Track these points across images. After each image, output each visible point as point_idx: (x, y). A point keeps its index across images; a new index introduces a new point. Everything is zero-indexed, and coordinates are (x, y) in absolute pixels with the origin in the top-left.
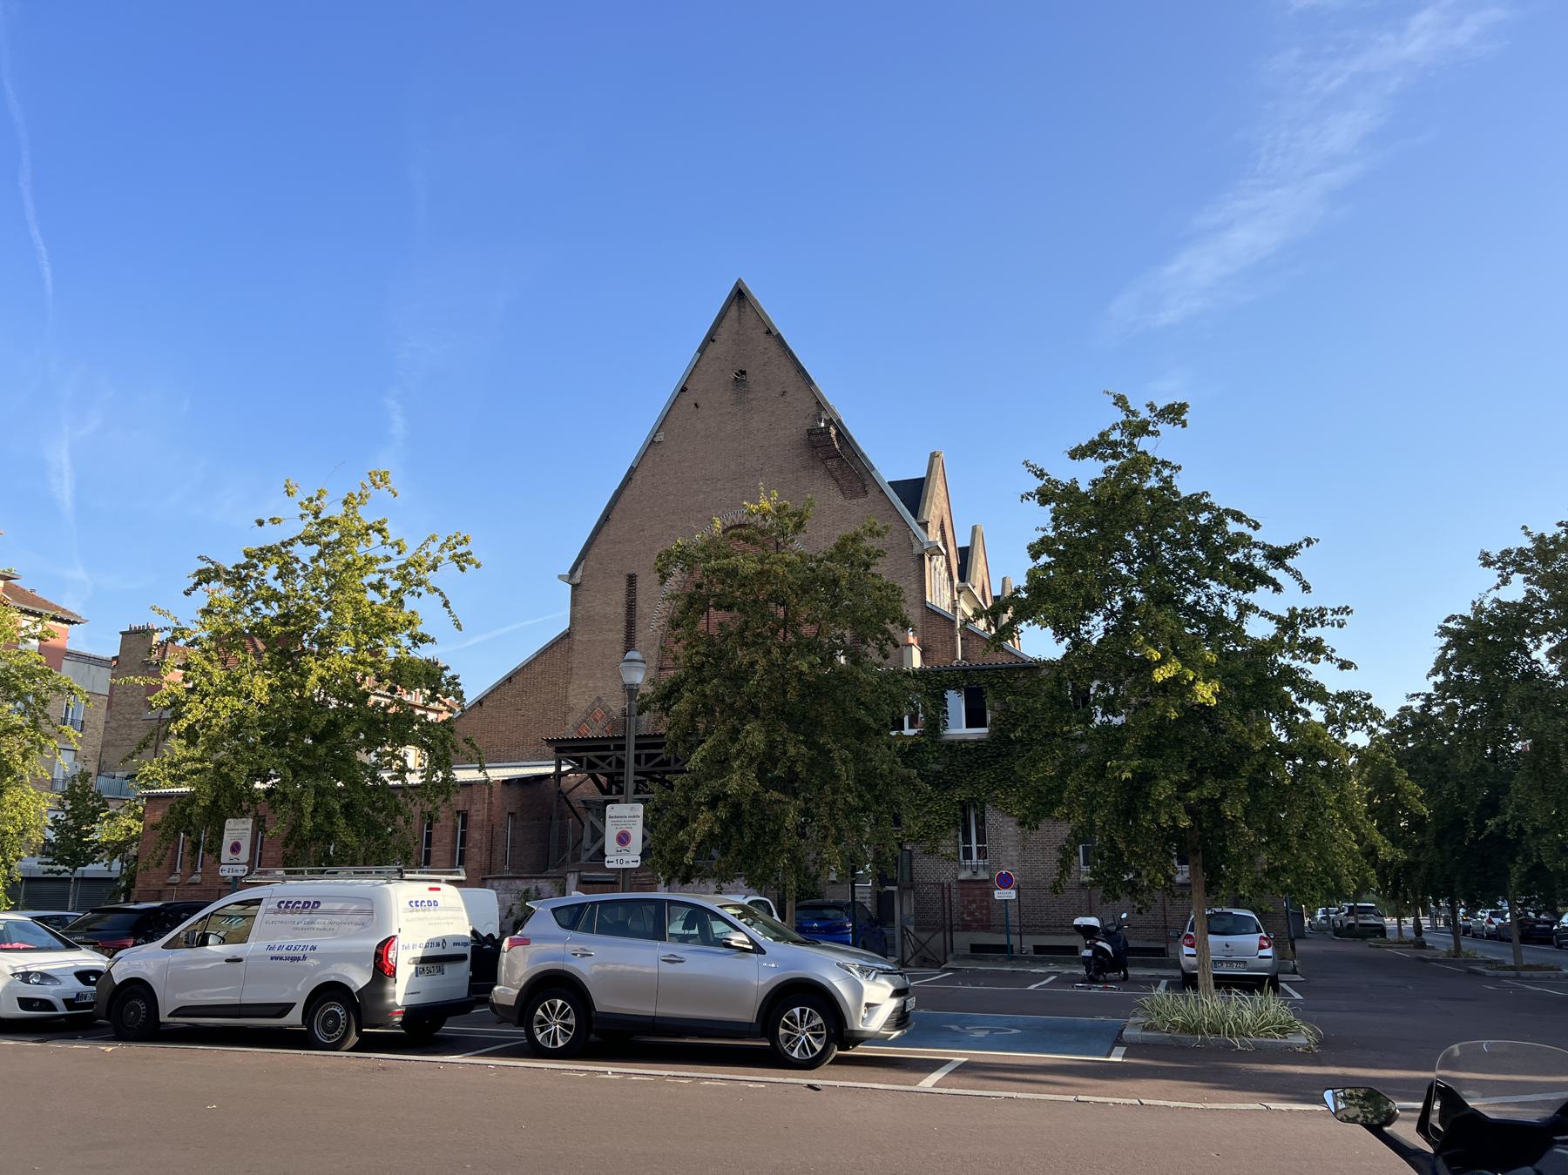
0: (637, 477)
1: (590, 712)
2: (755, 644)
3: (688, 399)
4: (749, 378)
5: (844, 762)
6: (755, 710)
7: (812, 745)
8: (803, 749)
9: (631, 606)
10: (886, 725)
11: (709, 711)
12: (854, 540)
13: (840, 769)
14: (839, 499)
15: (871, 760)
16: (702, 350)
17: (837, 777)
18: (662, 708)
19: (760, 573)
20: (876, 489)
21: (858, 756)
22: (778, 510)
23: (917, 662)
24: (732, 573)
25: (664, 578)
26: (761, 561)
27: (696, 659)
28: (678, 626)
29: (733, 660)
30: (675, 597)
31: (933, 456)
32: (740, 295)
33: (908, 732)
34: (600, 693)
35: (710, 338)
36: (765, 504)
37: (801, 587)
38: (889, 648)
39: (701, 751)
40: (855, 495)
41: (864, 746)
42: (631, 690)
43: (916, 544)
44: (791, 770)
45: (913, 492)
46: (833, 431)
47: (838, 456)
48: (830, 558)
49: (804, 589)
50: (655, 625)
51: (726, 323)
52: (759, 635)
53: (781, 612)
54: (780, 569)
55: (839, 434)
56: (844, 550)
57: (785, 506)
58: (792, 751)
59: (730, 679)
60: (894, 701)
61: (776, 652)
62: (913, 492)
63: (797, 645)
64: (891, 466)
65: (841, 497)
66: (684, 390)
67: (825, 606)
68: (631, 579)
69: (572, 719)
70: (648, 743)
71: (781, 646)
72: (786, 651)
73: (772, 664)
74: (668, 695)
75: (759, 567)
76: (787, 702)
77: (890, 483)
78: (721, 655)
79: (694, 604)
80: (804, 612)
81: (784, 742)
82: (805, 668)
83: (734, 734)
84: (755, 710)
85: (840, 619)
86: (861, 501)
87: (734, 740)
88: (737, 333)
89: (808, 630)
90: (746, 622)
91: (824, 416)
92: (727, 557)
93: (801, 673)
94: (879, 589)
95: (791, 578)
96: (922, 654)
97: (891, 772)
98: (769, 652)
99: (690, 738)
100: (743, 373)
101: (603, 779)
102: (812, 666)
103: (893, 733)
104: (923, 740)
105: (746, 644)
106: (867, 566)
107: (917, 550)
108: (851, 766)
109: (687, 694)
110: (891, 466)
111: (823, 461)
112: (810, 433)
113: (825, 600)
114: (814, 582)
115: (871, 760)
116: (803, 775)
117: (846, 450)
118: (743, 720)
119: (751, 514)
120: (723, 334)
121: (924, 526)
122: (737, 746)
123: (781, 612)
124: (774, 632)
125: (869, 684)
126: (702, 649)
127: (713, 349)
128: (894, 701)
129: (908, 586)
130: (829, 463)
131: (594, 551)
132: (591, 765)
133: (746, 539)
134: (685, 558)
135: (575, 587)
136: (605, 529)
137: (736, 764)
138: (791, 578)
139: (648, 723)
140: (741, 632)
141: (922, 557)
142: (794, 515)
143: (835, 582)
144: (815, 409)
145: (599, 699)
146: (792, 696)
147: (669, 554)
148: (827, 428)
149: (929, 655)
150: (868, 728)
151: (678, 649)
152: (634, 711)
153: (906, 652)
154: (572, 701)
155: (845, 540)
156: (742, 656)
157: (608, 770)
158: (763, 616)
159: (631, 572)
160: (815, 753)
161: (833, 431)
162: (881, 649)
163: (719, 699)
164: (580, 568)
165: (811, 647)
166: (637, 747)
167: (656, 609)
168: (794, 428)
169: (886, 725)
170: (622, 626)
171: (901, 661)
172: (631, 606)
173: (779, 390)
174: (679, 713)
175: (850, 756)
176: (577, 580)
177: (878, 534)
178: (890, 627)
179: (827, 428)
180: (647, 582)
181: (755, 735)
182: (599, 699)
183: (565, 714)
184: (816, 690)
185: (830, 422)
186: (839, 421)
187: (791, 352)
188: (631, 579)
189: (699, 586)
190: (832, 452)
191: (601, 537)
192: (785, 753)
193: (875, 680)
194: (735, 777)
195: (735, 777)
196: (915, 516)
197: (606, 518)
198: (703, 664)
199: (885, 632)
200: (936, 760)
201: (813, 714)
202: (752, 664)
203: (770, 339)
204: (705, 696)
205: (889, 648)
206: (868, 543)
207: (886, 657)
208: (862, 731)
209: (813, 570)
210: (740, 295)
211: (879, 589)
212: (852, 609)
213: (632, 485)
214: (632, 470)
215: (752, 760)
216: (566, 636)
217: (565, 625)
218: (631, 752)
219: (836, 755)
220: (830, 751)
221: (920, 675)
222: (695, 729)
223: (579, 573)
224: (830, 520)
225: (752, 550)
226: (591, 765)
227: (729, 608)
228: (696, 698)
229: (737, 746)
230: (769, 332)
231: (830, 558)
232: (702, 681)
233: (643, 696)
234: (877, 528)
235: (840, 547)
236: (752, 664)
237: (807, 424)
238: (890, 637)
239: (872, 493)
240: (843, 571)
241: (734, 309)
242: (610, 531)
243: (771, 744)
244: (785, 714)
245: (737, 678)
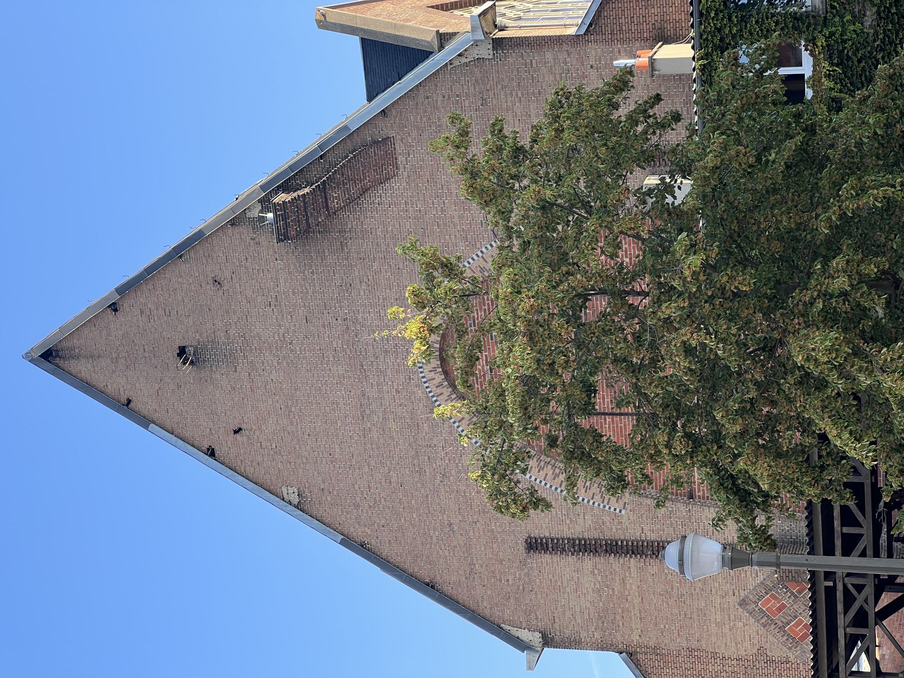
0: (359, 533)
1: (767, 619)
2: (653, 346)
3: (226, 446)
4: (190, 340)
5: (862, 191)
6: (769, 347)
7: (832, 248)
8: (837, 262)
9: (584, 547)
10: (798, 116)
11: (770, 424)
12: (474, 175)
13: (873, 198)
14: (397, 185)
15: (859, 144)
16: (144, 421)
17: (889, 202)
18: (765, 506)
19: (531, 337)
20: (380, 123)
21: (853, 166)
22: (421, 305)
23: (680, 53)
24: (530, 385)
25: (538, 502)
26: (510, 335)
27: (679, 448)
28: (621, 479)
29: (681, 384)
30: (572, 484)
31: (324, 24)
32: (49, 357)
33: (806, 68)
34: (733, 600)
35: (125, 407)
36: (413, 328)
37: (554, 267)
38: (660, 111)
39: (840, 440)
40: (391, 158)
41: (835, 154)
42: (735, 559)
43: (475, 53)
44: (875, 284)
45: (387, 59)
46: (282, 197)
47: (323, 188)
48: (505, 214)
49: (559, 260)
51: (99, 380)
52: (638, 337)
53: (600, 304)
54: (525, 303)
55: (286, 187)
56: (491, 192)
57: (416, 294)
58: (841, 282)
59: (714, 389)
60: (755, 104)
61: (669, 309)
62: (387, 59)
63: (656, 273)
64: (338, 98)
65: (394, 184)
66: (211, 453)
67: (590, 224)
68: (535, 545)
69: (778, 649)
70: (829, 530)
71: (658, 302)
72: (667, 292)
73: (688, 316)
74: (741, 494)
75: (521, 339)
76: (756, 291)
77: (370, 98)
78: (674, 406)
79: (582, 452)
80: (598, 261)
81: (827, 296)
82: (696, 260)
83: (811, 383)
84: (769, 347)
85: (611, 198)
86: (400, 148)
87: (822, 384)
88: (115, 361)
89: (630, 253)
90: (616, 360)
91: (255, 213)
92: (502, 394)
93: (705, 266)
94: (560, 131)
95: (541, 285)
96: (667, 40)
97: (882, 109)
98: (668, 321)
99: (818, 457)
100: (182, 351)
101: (886, 599)
102: (692, 248)
103: (809, 93)
104: (821, 41)
105: (654, 361)
106: (518, 151)
107: (485, 51)
108: (869, 179)
109: (741, 464)
110: (338, 98)
111: (332, 214)
112: (283, 237)
113: (579, 223)
114: (548, 242)
115: (859, 144)
116: (884, 262)
117: (314, 173)
118: (785, 367)
119: (428, 354)
120: (118, 385)
121: (443, 39)
122: (833, 377)
123: (600, 304)
124: (633, 312)
125: (725, 147)
126: (661, 438)
127: (144, 403)
128: (755, 104)
129: (552, 75)
130: (334, 204)
131: (485, 608)
132: (861, 619)
133: (472, 360)
134: (502, 467)
135: (548, 641)
136: (448, 590)
137: (865, 381)
138: (541, 285)
139: (788, 523)
140: (634, 370)
141: (498, 43)
142: (430, 278)
143: (545, 207)
144: (245, 232)
145: (743, 603)
146: (745, 282)
147: (496, 494)
148: (275, 208)
149: (669, 29)
150: (802, 149)
151: (663, 474)
152: (770, 556)
153: (663, 70)
154: (747, 649)
155: (472, 189)
156: (676, 366)
157: (869, 591)
158: (606, 332)
159: (522, 547)
160: (846, 243)
161: (282, 197)
162: (663, 126)
163: (748, 409)
164: (515, 632)
165: (659, 250)
166: (829, 551)
167: (595, 509)
168: (273, 266)
169: (798, 116)
170: (615, 563)
171: (680, 78)
172: (584, 547)
173: (210, 289)
174: (774, 478)
175: (852, 181)
176: (534, 638)
177: (464, 133)
178: (623, 112)
179: (275, 208)
180: (540, 524)
181: (812, 347)
182: (743, 603)
183: (769, 661)
184: (735, 248)
185: (265, 203)
186: (263, 188)
187: (150, 270)
188: (535, 545)
189: (553, 442)
190: (314, 200)
191: (462, 595)
192: (844, 294)
193: (718, 139)
194: (888, 382)
195: (888, 382)
196: (425, 55)
197: (430, 588)
198: (688, 436)
199: (633, 120)
200: (858, 18)
201: (776, 246)
202: (688, 350)
203: (125, 306)
204: (743, 433)
205: (660, 111)
206: (478, 149)
207: (677, 117)
208: (808, 160)
209: (525, 245)
210: (49, 357)
211: (560, 131)
212: (594, 178)
213: (373, 543)
214: (348, 542)
215: (857, 353)
216: (631, 656)
217: (615, 660)
218: (839, 562)
219: (850, 206)
220: (842, 216)
221: (713, 46)
222: (801, 450)
223: (525, 635)
224: (432, 210)
225: (494, 350)
226: (861, 619)
227: (590, 390)
228: (747, 450)
229: (833, 377)
230: (114, 307)
231: (505, 214)
232: (718, 437)
233: (744, 539)
234: (453, 134)
235: (487, 198)
236: (688, 350)
237: (268, 241)
238: (643, 111)
239: (387, 129)
240: (527, 194)
241: (74, 366)
242: (450, 578)
243: (830, 318)
244: (776, 297)
245: (713, 376)
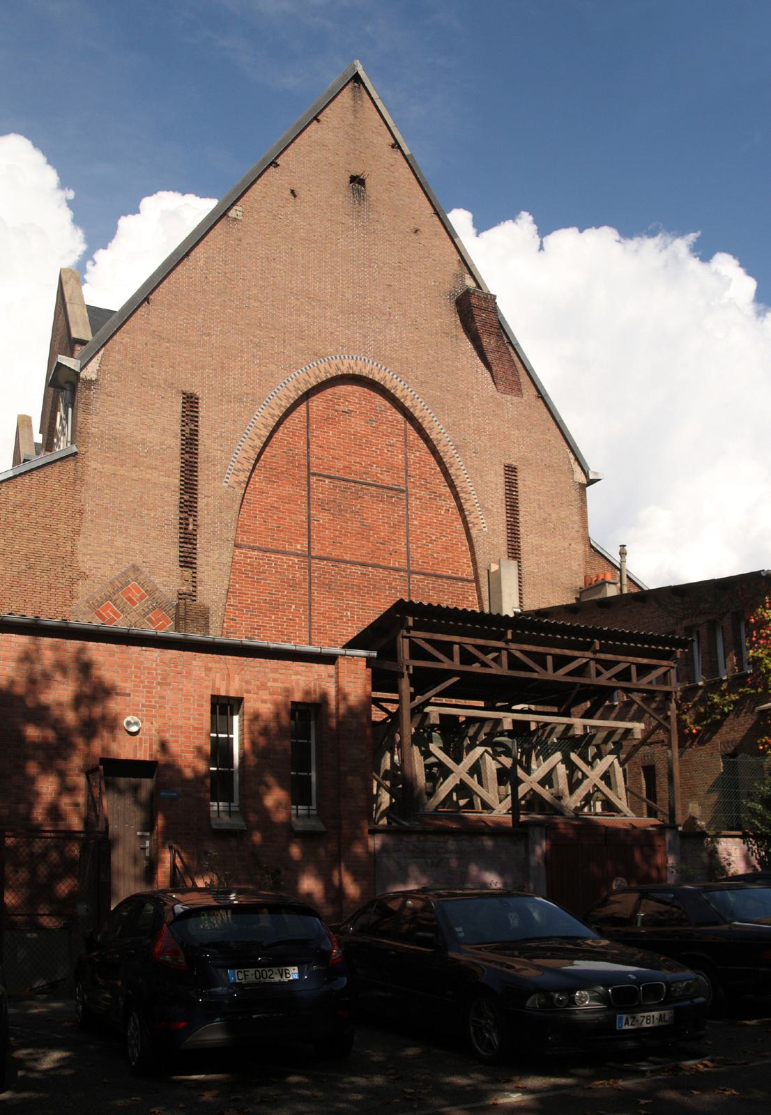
34: (138, 560)
50: (232, 479)
154: (85, 562)
182: (135, 568)
188: (190, 402)
